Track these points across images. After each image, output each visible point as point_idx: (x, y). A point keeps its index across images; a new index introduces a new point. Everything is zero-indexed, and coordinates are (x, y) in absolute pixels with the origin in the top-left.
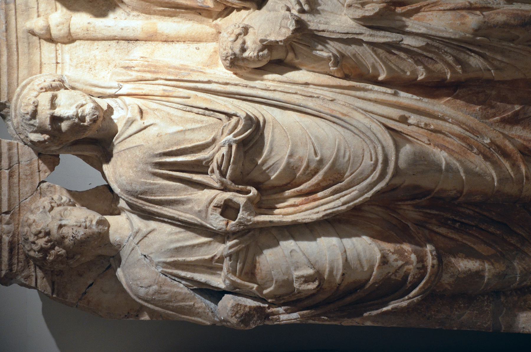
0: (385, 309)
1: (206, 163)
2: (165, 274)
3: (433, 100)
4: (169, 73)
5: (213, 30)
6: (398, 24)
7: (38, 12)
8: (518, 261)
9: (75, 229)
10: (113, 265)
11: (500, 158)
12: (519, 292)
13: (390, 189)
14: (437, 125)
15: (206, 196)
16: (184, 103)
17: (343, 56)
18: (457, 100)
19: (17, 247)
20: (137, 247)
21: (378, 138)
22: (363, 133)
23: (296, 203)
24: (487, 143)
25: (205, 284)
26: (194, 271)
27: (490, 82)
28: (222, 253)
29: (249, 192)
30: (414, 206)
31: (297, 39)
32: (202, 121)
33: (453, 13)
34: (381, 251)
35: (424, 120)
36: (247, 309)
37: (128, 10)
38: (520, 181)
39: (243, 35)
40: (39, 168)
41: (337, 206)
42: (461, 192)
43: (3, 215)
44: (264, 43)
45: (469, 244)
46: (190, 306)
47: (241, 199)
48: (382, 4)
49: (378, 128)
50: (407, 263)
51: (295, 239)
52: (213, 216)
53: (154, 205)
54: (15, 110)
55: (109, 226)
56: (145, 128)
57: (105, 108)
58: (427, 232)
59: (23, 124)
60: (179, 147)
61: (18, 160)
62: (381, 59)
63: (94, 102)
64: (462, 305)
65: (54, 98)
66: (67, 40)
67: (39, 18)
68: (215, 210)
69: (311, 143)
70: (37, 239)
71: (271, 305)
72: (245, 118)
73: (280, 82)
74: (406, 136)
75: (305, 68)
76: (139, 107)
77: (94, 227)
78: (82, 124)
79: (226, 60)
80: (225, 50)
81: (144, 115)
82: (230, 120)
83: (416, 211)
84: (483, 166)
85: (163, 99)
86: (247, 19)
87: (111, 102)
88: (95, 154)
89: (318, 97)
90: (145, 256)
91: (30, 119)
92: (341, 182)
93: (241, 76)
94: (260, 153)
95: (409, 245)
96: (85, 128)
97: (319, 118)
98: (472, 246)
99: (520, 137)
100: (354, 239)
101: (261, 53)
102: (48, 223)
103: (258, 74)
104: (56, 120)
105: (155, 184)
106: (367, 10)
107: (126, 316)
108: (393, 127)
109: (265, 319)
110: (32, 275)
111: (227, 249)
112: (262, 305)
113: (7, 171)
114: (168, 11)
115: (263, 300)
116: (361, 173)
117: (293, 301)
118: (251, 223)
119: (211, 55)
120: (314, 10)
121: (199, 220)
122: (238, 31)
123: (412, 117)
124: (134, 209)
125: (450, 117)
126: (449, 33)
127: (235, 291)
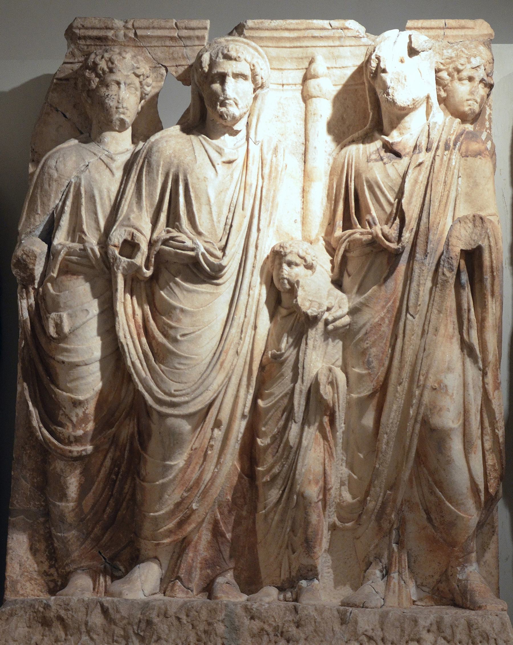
0: (30, 404)
1: (177, 226)
2: (69, 185)
3: (237, 454)
4: (268, 190)
5: (313, 237)
6: (312, 418)
7: (332, 68)
8: (76, 534)
9: (115, 97)
10: (82, 136)
11: (178, 519)
12: (48, 535)
13: (148, 410)
14: (212, 457)
15: (144, 226)
16: (238, 204)
17: (282, 363)
18: (237, 476)
19: (102, 44)
20: (96, 158)
21: (197, 397)
22: (203, 383)
23: (136, 316)
24: (192, 506)
25: (58, 225)
26: (71, 214)
27: (254, 510)
28: (88, 242)
29: (147, 268)
30: (132, 435)
31: (299, 318)
32: (219, 222)
33: (321, 473)
34: (87, 400)
35: (217, 445)
36: (31, 266)
37: (334, 154)
38: (154, 538)
39: (304, 264)
40: (180, 65)
41: (131, 356)
42: (143, 481)
43: (134, 31)
44: (296, 285)
45: (94, 488)
46: (37, 210)
47: (140, 260)
48: (331, 402)
49: (208, 398)
50: (74, 426)
51: (100, 315)
52: (123, 232)
53: (137, 174)
54: (233, 40)
55: (119, 131)
56: (213, 166)
57: (236, 128)
58: (106, 446)
59: (219, 47)
60: (193, 199)
61: (187, 46)
62: (278, 402)
63: (241, 117)
64: (35, 481)
65: (244, 77)
66: (305, 94)
67: (326, 69)
68: (130, 234)
69: (195, 330)
70: (106, 61)
71: (36, 291)
72: (221, 265)
73: (258, 302)
74: (201, 426)
75: (272, 326)
76: (235, 160)
77: (117, 116)
78: (219, 103)
79: (281, 246)
80: (290, 246)
81: (227, 165)
82: (219, 249)
83: (127, 436)
84: (170, 502)
85: (243, 184)
86: (322, 270)
87: (243, 134)
88: (191, 119)
89: (241, 338)
90: (88, 166)
91: (223, 54)
92: (155, 360)
93: (265, 263)
94: (186, 280)
95: (92, 428)
96: (215, 107)
97: (219, 339)
98: (92, 491)
99: (200, 538)
100: (99, 374)
101: (286, 282)
102: (122, 71)
103: (266, 280)
104: (222, 78)
105: (158, 175)
106: (325, 387)
107: (33, 150)
108: (210, 413)
109: (23, 284)
110: (75, 59)
111: (91, 246)
112: (37, 282)
113: (176, 35)
114: (332, 193)
115: (41, 283)
116: (162, 380)
117: (40, 313)
118: (116, 270)
119: (288, 234)
120: (328, 335)
121: (121, 219)
122: (309, 259)
123: (220, 433)
124: (135, 156)
125: (220, 470)
126: (301, 469)
127: (51, 255)
